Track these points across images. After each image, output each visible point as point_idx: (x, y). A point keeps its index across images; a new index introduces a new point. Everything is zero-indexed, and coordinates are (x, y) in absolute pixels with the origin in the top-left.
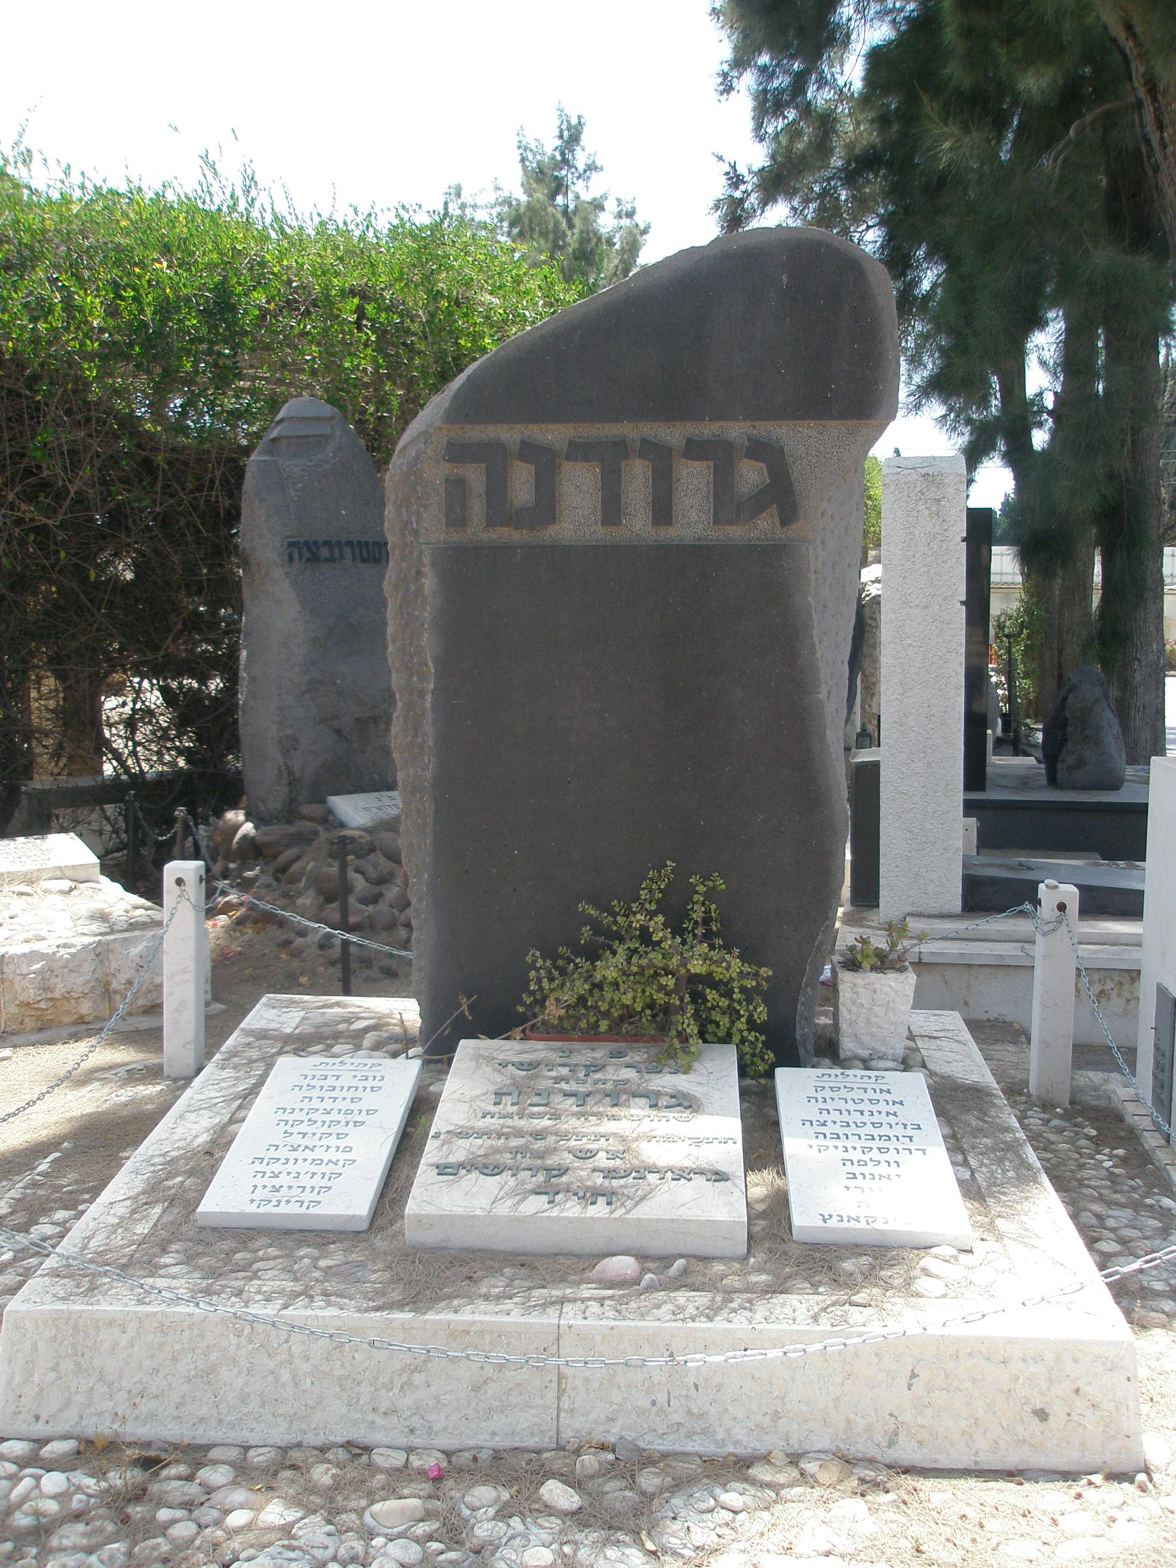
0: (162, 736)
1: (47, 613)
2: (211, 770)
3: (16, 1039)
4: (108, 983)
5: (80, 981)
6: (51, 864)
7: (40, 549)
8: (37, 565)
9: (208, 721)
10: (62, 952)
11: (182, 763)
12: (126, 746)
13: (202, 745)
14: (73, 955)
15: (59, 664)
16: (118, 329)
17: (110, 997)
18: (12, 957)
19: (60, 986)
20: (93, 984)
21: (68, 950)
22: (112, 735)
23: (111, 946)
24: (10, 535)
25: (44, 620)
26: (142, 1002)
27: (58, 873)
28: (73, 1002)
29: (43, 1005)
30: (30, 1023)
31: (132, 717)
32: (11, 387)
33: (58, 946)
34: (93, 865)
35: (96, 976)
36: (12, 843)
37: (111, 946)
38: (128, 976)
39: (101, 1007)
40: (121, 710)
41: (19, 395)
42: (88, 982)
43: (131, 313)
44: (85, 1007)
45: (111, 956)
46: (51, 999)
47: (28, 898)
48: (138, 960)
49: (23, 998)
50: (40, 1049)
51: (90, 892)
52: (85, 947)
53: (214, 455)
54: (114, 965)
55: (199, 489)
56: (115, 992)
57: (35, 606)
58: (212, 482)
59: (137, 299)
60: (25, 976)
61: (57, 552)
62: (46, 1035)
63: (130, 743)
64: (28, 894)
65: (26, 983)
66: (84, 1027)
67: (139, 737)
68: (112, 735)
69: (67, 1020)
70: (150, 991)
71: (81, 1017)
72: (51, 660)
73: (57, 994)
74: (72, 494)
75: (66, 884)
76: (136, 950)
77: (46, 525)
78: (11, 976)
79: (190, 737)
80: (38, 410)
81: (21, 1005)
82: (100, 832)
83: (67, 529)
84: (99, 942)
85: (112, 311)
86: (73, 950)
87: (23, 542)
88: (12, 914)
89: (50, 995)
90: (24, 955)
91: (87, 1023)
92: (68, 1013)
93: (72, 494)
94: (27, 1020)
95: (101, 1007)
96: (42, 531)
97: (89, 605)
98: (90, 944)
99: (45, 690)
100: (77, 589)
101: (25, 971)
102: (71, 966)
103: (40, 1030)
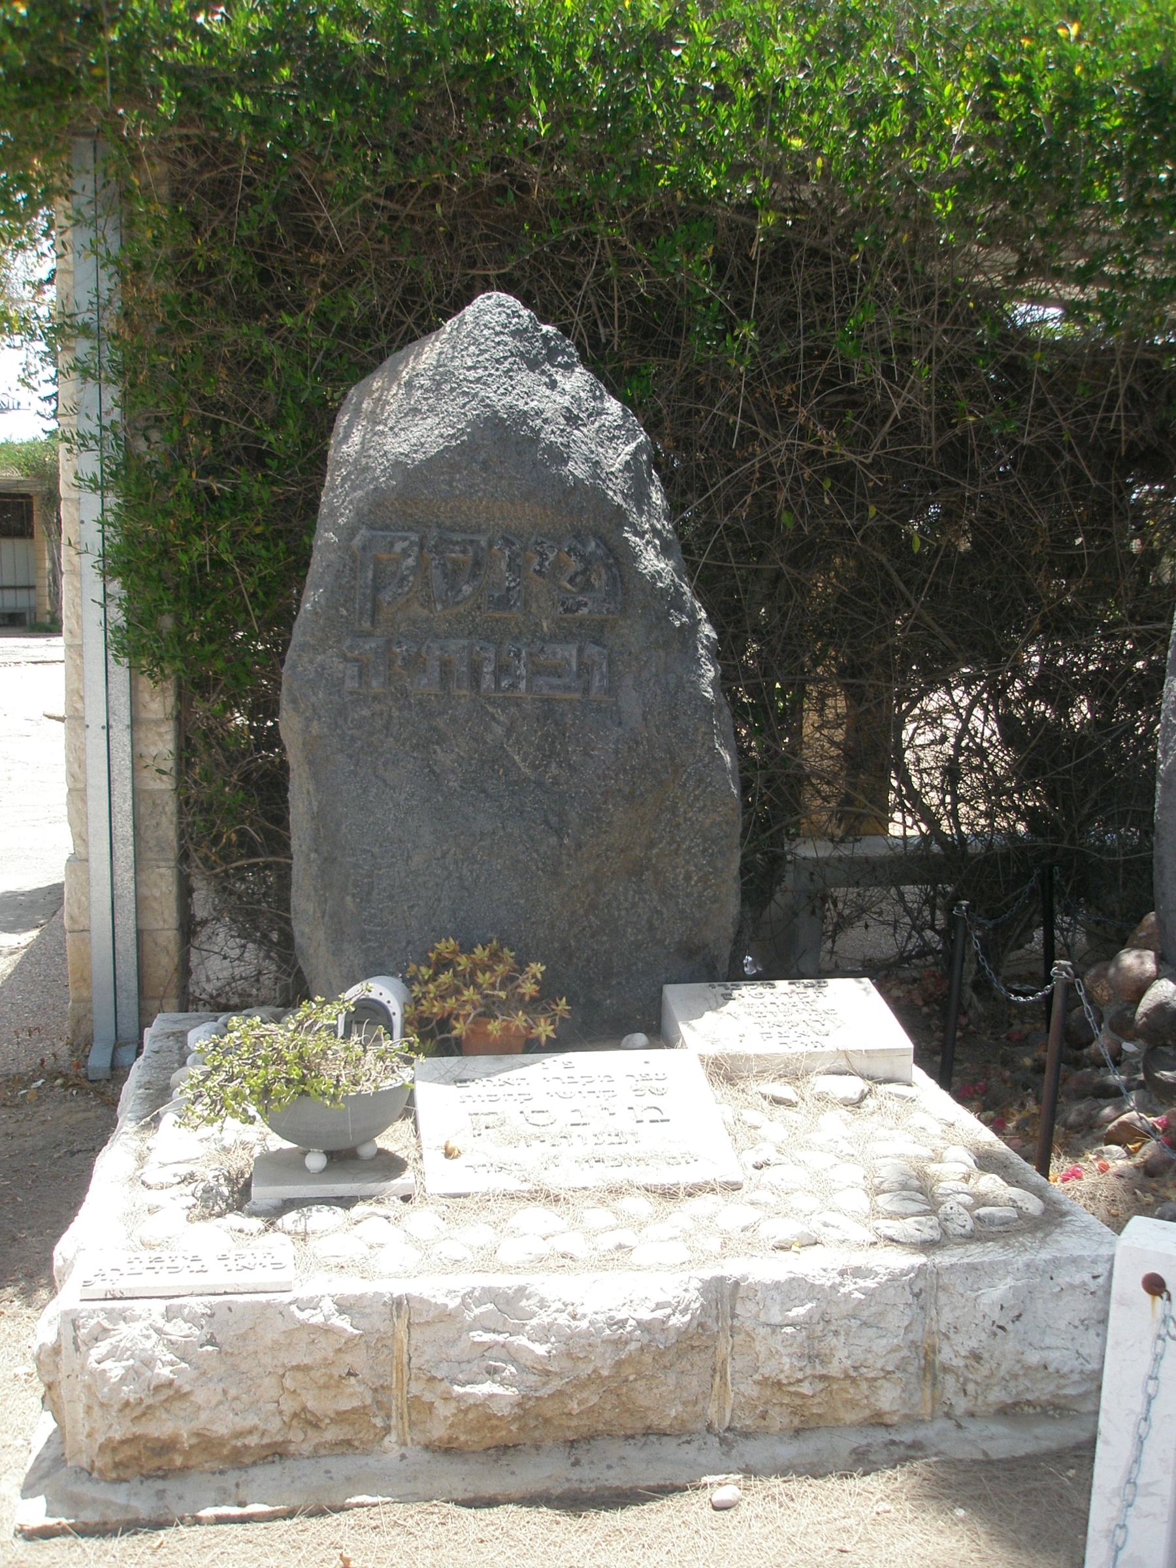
0: (994, 789)
1: (842, 599)
2: (1065, 844)
3: (753, 1451)
4: (934, 1350)
5: (880, 1346)
6: (830, 1045)
7: (842, 503)
8: (832, 526)
9: (1067, 771)
10: (849, 1286)
11: (1021, 827)
12: (943, 802)
13: (1053, 806)
14: (870, 1294)
15: (853, 676)
16: (990, 139)
17: (935, 1377)
18: (754, 1289)
19: (841, 1353)
20: (905, 1352)
21: (862, 1283)
22: (923, 785)
23: (945, 1279)
24: (796, 479)
25: (836, 610)
26: (997, 1395)
27: (842, 1064)
28: (864, 1386)
29: (806, 1389)
30: (779, 1419)
31: (952, 760)
32: (814, 244)
33: (842, 1273)
34: (901, 1052)
35: (911, 1336)
36: (766, 991)
37: (945, 1279)
38: (973, 1343)
39: (916, 1398)
40: (938, 748)
41: (826, 258)
42: (898, 1348)
43: (1013, 109)
44: (888, 1399)
45: (943, 1298)
46: (823, 1378)
47: (789, 1113)
48: (996, 1315)
49: (768, 1369)
50: (796, 1486)
51: (893, 1105)
52: (894, 1278)
53: (1119, 356)
54: (947, 1316)
55: (1093, 407)
56: (946, 1369)
57: (825, 588)
58: (1113, 397)
59: (1026, 89)
60: (775, 1328)
61: (863, 507)
62: (807, 1447)
63: (948, 799)
64: (790, 1104)
65: (776, 1343)
66: (882, 1436)
67: (962, 789)
68: (923, 785)
69: (850, 1417)
70: (1015, 1377)
71: (879, 1414)
72: (842, 671)
73: (834, 1369)
74: (897, 411)
75: (852, 1086)
76: (996, 1292)
77: (851, 464)
78: (749, 1325)
79: (1035, 792)
80: (853, 280)
81: (764, 1383)
82: (895, 925)
83: (881, 471)
84: (921, 1270)
85: (985, 110)
86: (870, 1283)
87: (815, 490)
88: (760, 1159)
89: (820, 1370)
90: (777, 1285)
91: (887, 1426)
92: (852, 1404)
93: (897, 411)
94: (774, 1412)
95: (916, 1398)
96: (843, 474)
97: (902, 587)
98: (904, 1273)
99: (830, 714)
100: (888, 565)
101: (777, 1319)
102: (865, 1314)
103: (798, 1432)
